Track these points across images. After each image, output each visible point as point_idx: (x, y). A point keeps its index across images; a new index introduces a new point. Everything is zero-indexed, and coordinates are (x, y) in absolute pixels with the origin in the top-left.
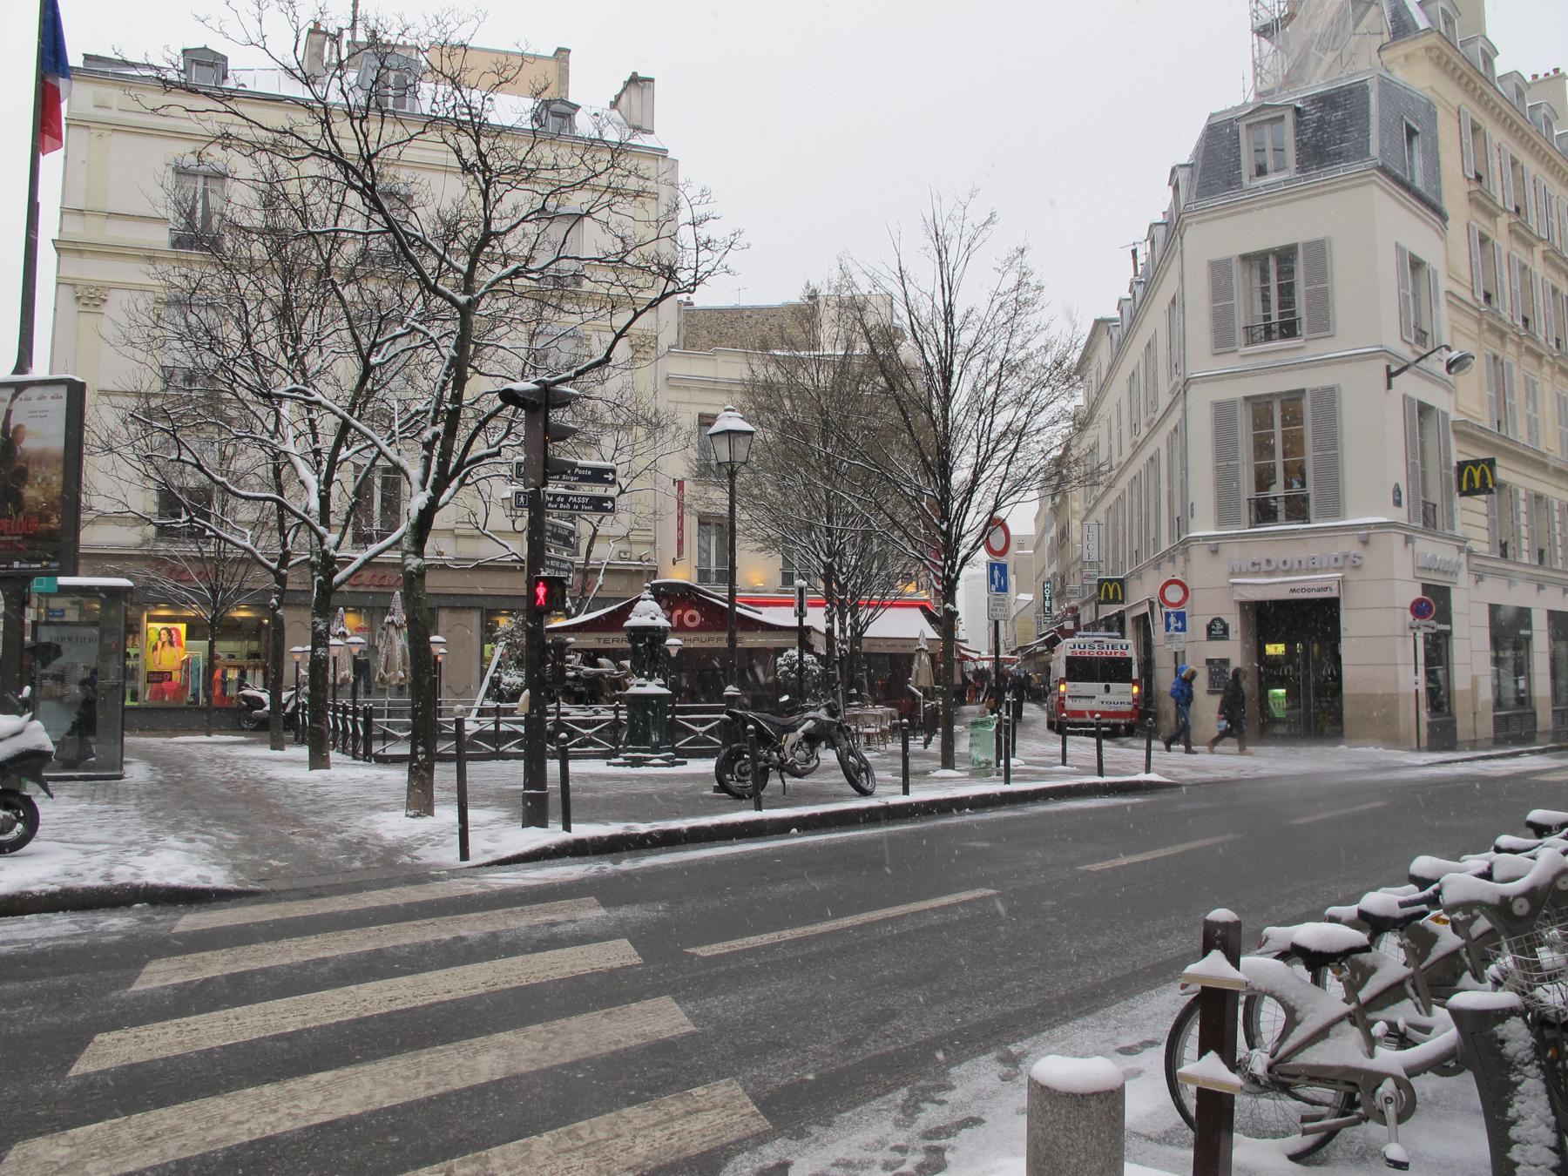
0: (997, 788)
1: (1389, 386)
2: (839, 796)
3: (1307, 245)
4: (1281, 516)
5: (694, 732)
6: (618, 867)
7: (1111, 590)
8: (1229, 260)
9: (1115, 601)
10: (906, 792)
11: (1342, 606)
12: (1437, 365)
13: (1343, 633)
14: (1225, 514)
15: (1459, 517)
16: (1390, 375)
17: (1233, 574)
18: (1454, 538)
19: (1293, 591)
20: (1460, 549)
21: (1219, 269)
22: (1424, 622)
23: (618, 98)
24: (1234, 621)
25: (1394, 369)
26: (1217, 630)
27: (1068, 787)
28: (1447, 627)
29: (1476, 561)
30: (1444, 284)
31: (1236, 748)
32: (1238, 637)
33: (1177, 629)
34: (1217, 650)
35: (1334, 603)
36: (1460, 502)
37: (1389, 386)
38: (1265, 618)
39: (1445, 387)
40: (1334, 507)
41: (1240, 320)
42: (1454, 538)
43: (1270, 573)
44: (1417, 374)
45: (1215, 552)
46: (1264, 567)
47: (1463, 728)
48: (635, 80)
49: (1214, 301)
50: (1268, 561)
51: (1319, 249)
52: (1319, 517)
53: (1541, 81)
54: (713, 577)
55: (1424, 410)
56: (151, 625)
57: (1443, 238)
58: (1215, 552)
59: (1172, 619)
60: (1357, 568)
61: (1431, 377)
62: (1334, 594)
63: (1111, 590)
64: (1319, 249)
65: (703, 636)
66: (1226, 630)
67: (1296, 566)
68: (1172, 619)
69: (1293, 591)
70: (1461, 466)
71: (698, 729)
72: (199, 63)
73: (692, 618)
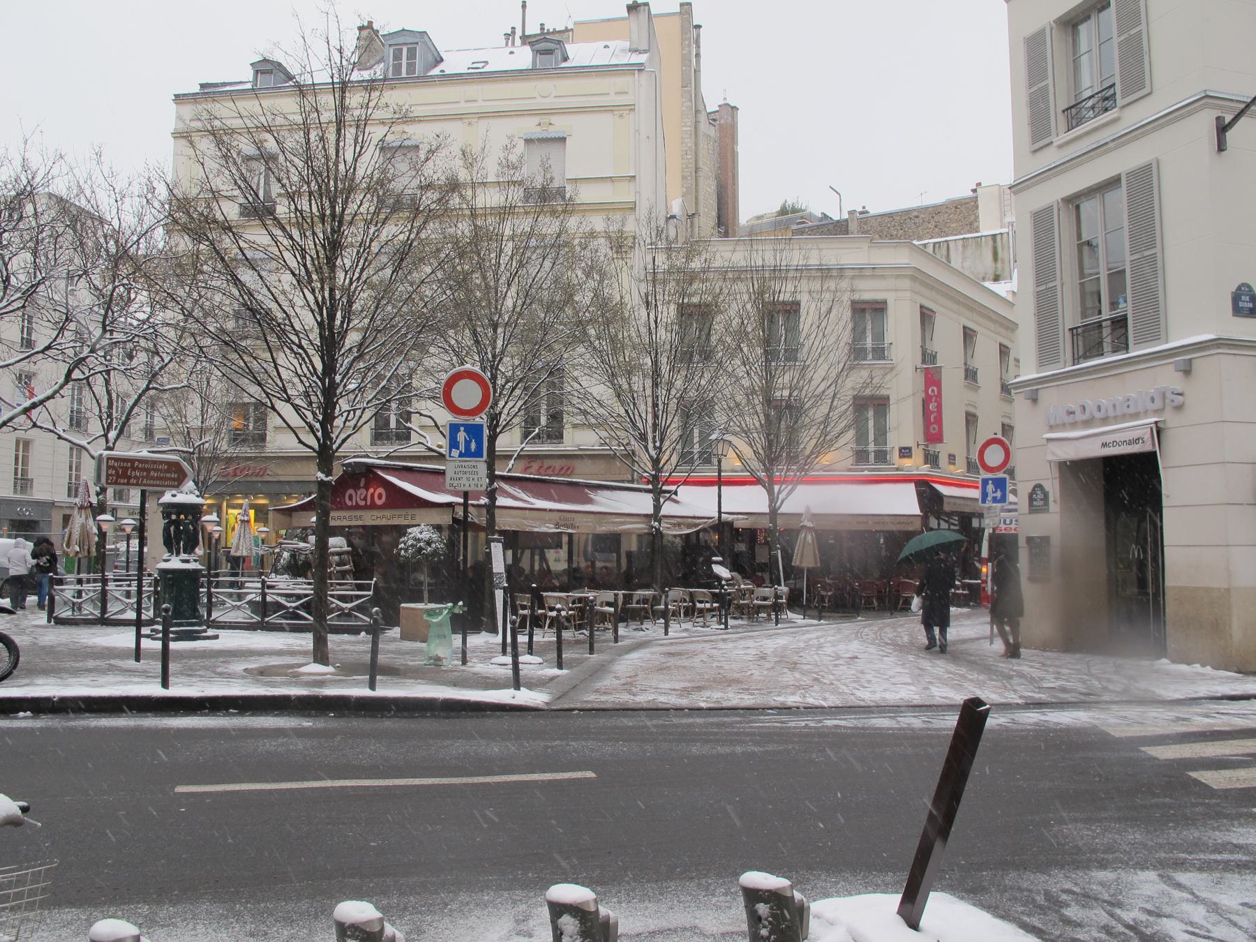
0: (154, 689)
1: (1221, 147)
2: (495, 684)
4: (1107, 347)
5: (285, 607)
10: (372, 687)
13: (1164, 503)
14: (1046, 352)
16: (1222, 129)
17: (1052, 428)
19: (1104, 445)
24: (1053, 487)
27: (286, 698)
33: (995, 500)
37: (1221, 147)
40: (1154, 331)
43: (1087, 423)
45: (1035, 400)
46: (1079, 417)
49: (1030, 86)
50: (1099, 408)
52: (1141, 341)
54: (872, 456)
56: (230, 511)
58: (1035, 400)
59: (990, 487)
60: (1179, 408)
62: (1146, 447)
65: (388, 513)
68: (990, 487)
69: (1104, 445)
71: (344, 605)
72: (263, 72)
73: (380, 496)
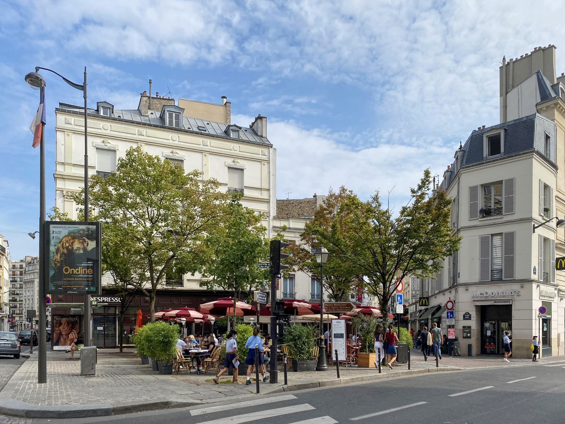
3: (506, 181)
6: (164, 396)
7: (424, 301)
8: (476, 187)
9: (425, 305)
11: (513, 308)
12: (553, 224)
13: (513, 318)
15: (557, 277)
18: (554, 285)
20: (556, 289)
21: (473, 190)
22: (543, 315)
23: (253, 124)
24: (473, 314)
25: (536, 226)
26: (467, 317)
28: (550, 316)
29: (561, 293)
30: (555, 193)
31: (423, 358)
32: (475, 319)
34: (467, 323)
35: (551, 48)
36: (557, 272)
38: (485, 312)
39: (553, 231)
41: (479, 208)
42: (554, 285)
44: (544, 227)
47: (473, 354)
49: (471, 201)
51: (511, 182)
53: (537, 51)
55: (546, 240)
57: (556, 177)
59: (449, 314)
61: (549, 228)
63: (424, 301)
64: (511, 182)
66: (470, 317)
67: (497, 295)
68: (449, 314)
70: (558, 259)
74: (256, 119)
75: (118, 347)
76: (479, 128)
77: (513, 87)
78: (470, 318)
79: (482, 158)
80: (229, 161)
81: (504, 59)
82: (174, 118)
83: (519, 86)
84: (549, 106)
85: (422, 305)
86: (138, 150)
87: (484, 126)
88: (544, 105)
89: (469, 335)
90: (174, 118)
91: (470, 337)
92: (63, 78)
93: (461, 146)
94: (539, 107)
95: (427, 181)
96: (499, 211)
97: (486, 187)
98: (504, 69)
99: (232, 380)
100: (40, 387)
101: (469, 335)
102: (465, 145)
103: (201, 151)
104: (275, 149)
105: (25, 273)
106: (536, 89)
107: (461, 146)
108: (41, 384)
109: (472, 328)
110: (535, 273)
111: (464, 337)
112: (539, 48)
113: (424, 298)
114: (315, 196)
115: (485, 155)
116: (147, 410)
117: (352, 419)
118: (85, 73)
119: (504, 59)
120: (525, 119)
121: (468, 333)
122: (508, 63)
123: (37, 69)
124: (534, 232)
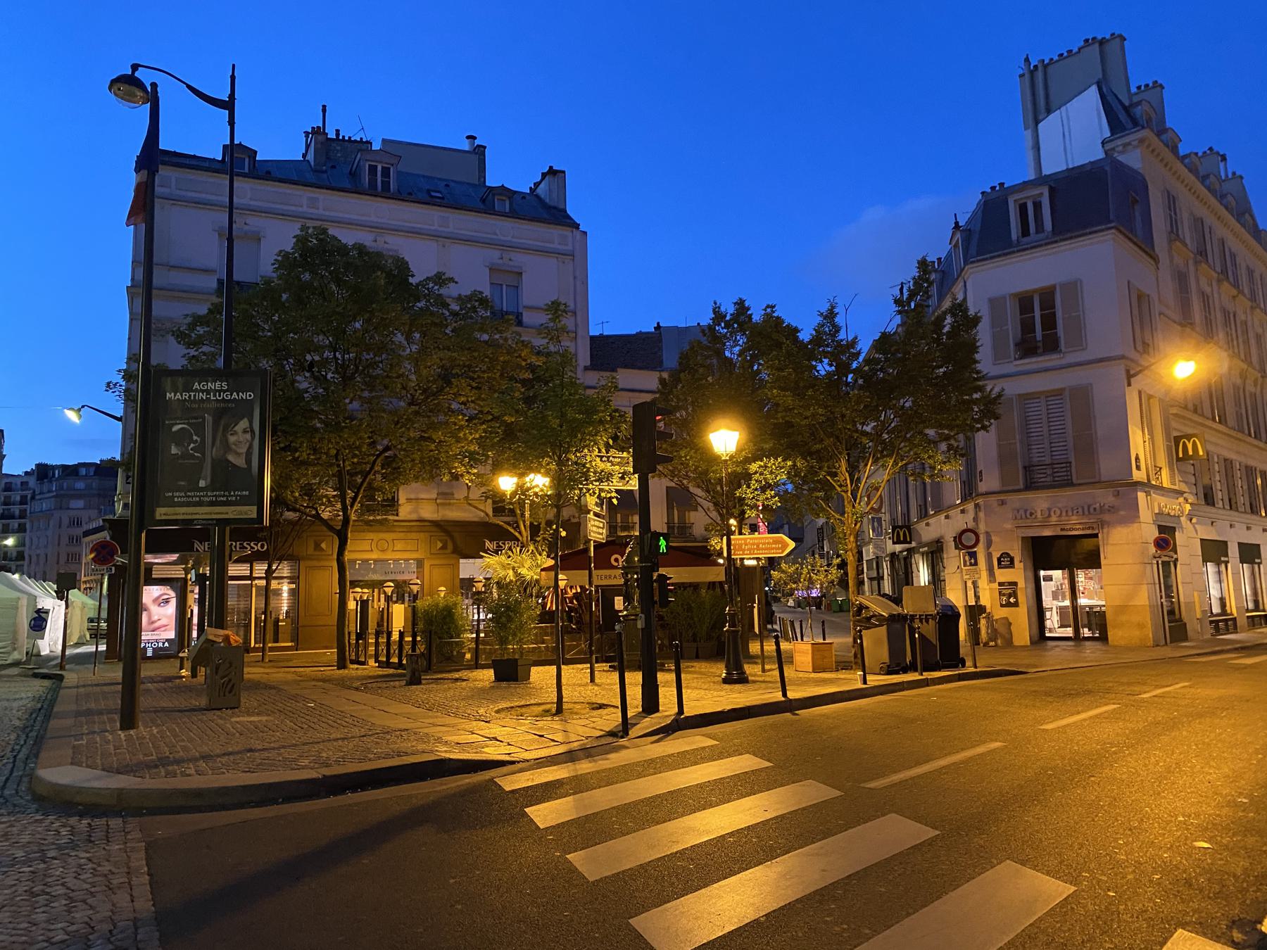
9: (905, 542)
22: (1165, 553)
24: (1017, 554)
48: (552, 172)
51: (1073, 288)
64: (1073, 288)
74: (544, 175)
75: (255, 650)
76: (993, 188)
77: (1049, 111)
78: (1011, 564)
79: (1009, 244)
80: (494, 255)
81: (1027, 60)
82: (379, 174)
83: (1063, 109)
84: (1129, 144)
85: (898, 542)
86: (324, 231)
87: (1002, 184)
88: (1119, 142)
89: (1012, 600)
90: (379, 174)
91: (1016, 604)
92: (189, 87)
93: (957, 223)
94: (1108, 147)
95: (927, 280)
96: (1052, 345)
97: (1025, 302)
98: (1027, 76)
99: (554, 710)
100: (129, 738)
101: (1012, 600)
102: (970, 221)
103: (435, 236)
104: (585, 233)
105: (33, 498)
106: (1098, 110)
107: (957, 223)
108: (127, 733)
109: (1019, 586)
110: (1138, 468)
111: (1002, 606)
112: (1094, 39)
113: (901, 527)
114: (658, 327)
115: (1014, 236)
116: (198, 793)
117: (872, 785)
118: (233, 78)
119: (1027, 60)
120: (1089, 168)
121: (1010, 596)
122: (1036, 67)
123: (135, 67)
124: (1129, 385)
